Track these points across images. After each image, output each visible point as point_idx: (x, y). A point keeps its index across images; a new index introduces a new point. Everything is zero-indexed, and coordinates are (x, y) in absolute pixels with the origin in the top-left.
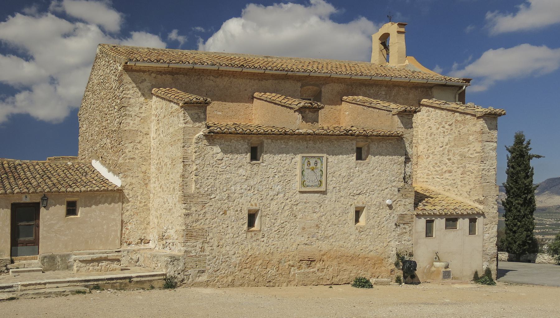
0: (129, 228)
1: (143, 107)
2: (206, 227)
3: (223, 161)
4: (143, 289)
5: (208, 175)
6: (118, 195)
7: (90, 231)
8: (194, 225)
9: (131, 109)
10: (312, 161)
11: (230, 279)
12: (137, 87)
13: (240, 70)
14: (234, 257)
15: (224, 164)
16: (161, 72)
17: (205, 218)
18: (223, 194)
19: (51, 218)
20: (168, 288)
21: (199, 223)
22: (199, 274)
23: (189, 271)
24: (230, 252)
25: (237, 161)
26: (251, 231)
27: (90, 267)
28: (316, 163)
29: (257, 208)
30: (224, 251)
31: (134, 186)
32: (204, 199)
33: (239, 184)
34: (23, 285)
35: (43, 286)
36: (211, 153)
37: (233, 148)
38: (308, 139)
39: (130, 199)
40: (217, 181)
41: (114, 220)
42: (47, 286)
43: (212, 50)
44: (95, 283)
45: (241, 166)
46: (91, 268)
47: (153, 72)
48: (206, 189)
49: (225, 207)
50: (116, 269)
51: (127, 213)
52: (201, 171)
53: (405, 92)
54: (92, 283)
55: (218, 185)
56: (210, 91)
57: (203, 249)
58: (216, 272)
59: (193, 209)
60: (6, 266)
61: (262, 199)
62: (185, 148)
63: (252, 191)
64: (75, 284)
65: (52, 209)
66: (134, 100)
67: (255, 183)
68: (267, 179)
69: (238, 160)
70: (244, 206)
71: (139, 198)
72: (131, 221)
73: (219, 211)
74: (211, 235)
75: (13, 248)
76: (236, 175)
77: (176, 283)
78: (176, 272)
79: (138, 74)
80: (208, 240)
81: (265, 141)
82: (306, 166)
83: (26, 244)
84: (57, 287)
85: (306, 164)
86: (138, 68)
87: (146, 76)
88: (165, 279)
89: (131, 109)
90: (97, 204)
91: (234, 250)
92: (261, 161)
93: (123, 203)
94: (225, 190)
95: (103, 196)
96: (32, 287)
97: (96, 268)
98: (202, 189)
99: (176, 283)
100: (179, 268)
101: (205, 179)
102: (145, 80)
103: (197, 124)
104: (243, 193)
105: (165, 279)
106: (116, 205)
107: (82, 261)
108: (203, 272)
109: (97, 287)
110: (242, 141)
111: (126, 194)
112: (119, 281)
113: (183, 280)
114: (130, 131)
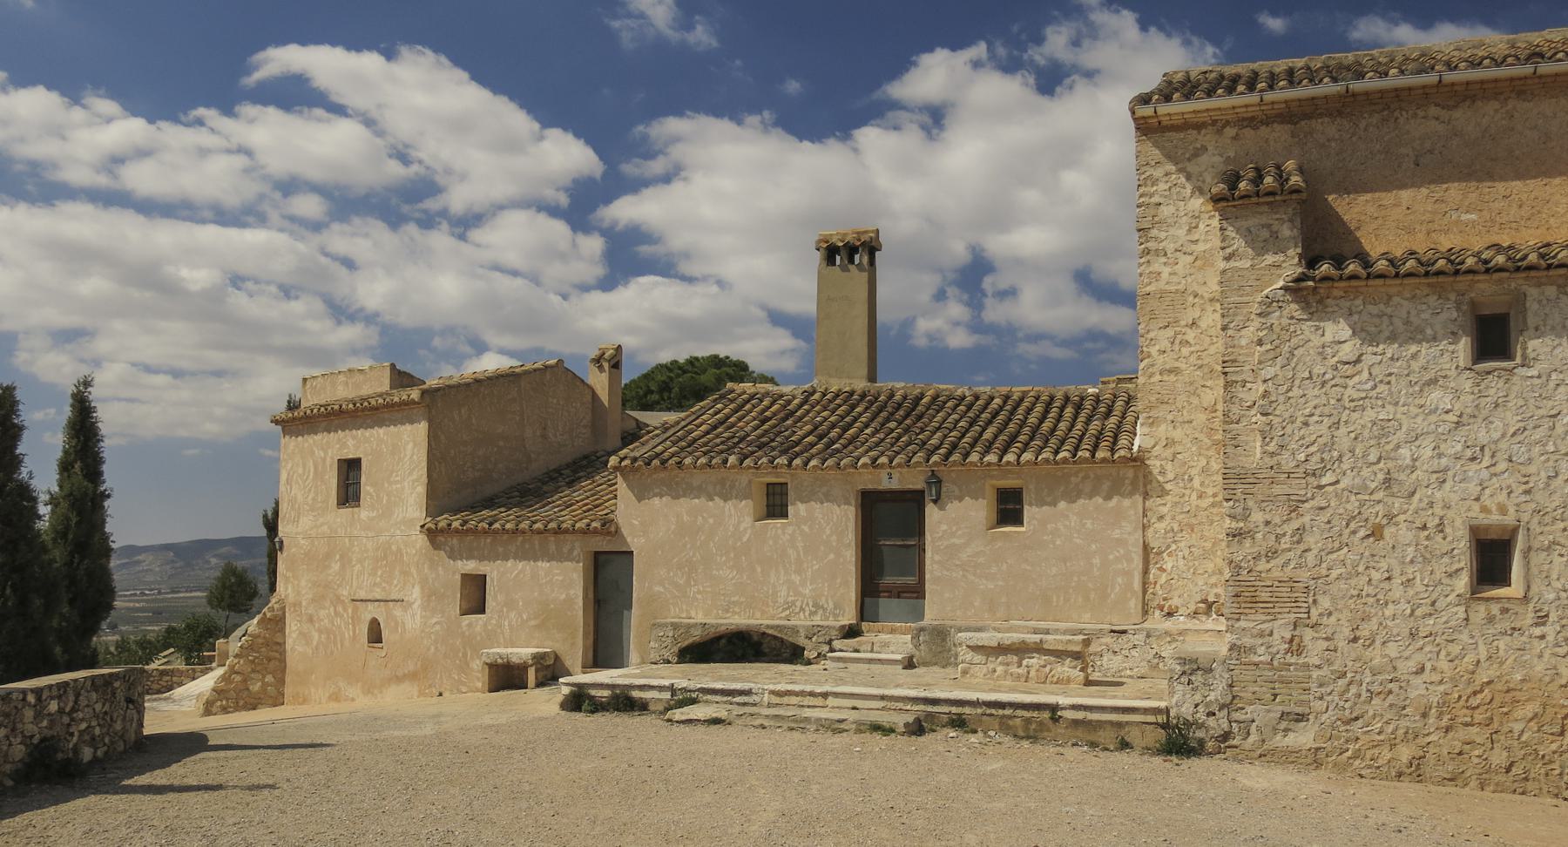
0: (1168, 566)
1: (1201, 226)
2: (1304, 575)
3: (1364, 365)
4: (1093, 745)
5: (1307, 411)
6: (1130, 473)
7: (1054, 570)
8: (1262, 565)
9: (1163, 235)
11: (1405, 753)
12: (1180, 171)
13: (1528, 69)
14: (1417, 681)
15: (1365, 375)
16: (1252, 119)
17: (1302, 547)
18: (1366, 472)
19: (954, 528)
20: (1170, 753)
21: (1279, 561)
22: (1284, 725)
23: (1249, 709)
24: (1400, 664)
25: (1415, 365)
26: (1488, 599)
27: (997, 665)
29: (1510, 520)
30: (1376, 656)
31: (1179, 448)
32: (1296, 487)
33: (1431, 438)
34: (772, 692)
35: (819, 701)
36: (1316, 341)
37: (1398, 322)
39: (1168, 487)
40: (1343, 430)
41: (1121, 542)
42: (831, 701)
43: (1063, 29)
44: (954, 710)
45: (1433, 382)
46: (1000, 669)
47: (1228, 123)
48: (1302, 457)
49: (1376, 513)
50: (1069, 681)
51: (1161, 526)
52: (1281, 399)
54: (945, 709)
55: (1344, 442)
56: (1431, 152)
57: (1295, 646)
58: (1348, 722)
59: (1257, 517)
60: (830, 642)
61: (1527, 492)
62: (1230, 332)
63: (1486, 461)
64: (900, 705)
65: (953, 508)
66: (1172, 209)
67: (1496, 435)
68: (1547, 423)
69: (1422, 361)
70: (1450, 514)
71: (1196, 483)
72: (1174, 547)
73: (1353, 526)
74: (1325, 602)
75: (867, 600)
76: (1414, 410)
77: (1201, 742)
78: (1201, 709)
79: (1182, 135)
80: (1314, 618)
83: (898, 593)
84: (854, 708)
86: (1177, 120)
87: (1207, 138)
88: (1165, 726)
89: (1163, 235)
90: (1072, 496)
91: (1419, 657)
92: (1518, 360)
93: (1146, 496)
94: (1372, 458)
95: (1086, 477)
96: (794, 700)
97: (1014, 669)
98: (1286, 455)
99: (1201, 742)
100: (1212, 697)
101: (1298, 424)
103: (1270, 259)
104: (1446, 470)
105: (1165, 726)
106: (1127, 502)
107: (976, 649)
108: (1301, 718)
109: (959, 723)
110: (1432, 300)
111: (1155, 472)
112: (1020, 713)
113: (1226, 736)
114: (1162, 295)
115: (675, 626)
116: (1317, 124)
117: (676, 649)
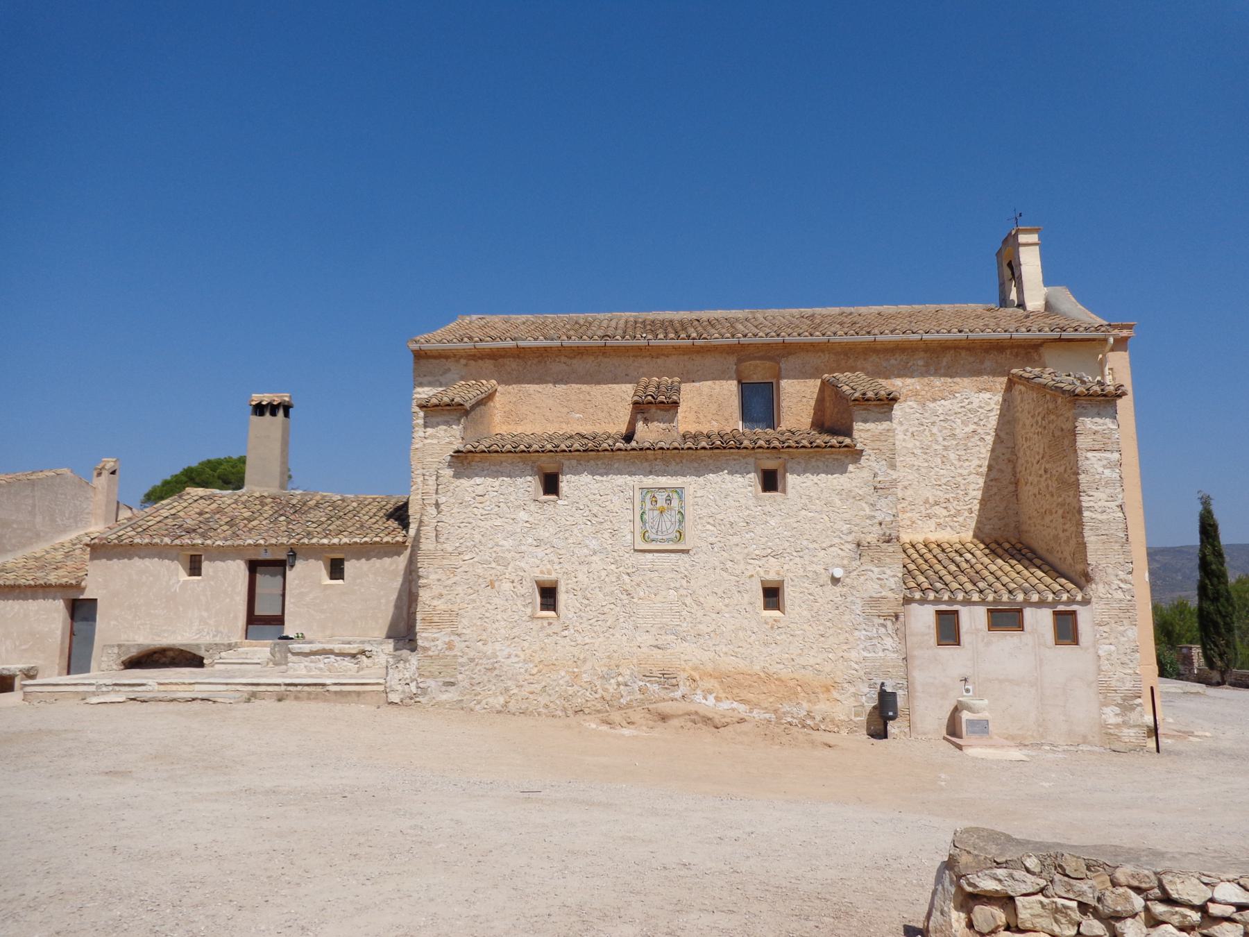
8: (435, 603)
10: (661, 497)
28: (669, 500)
38: (651, 457)
53: (972, 359)
81: (566, 463)
82: (648, 505)
85: (648, 502)
102: (449, 370)
108: (452, 684)
115: (119, 646)
116: (507, 361)
117: (120, 661)
